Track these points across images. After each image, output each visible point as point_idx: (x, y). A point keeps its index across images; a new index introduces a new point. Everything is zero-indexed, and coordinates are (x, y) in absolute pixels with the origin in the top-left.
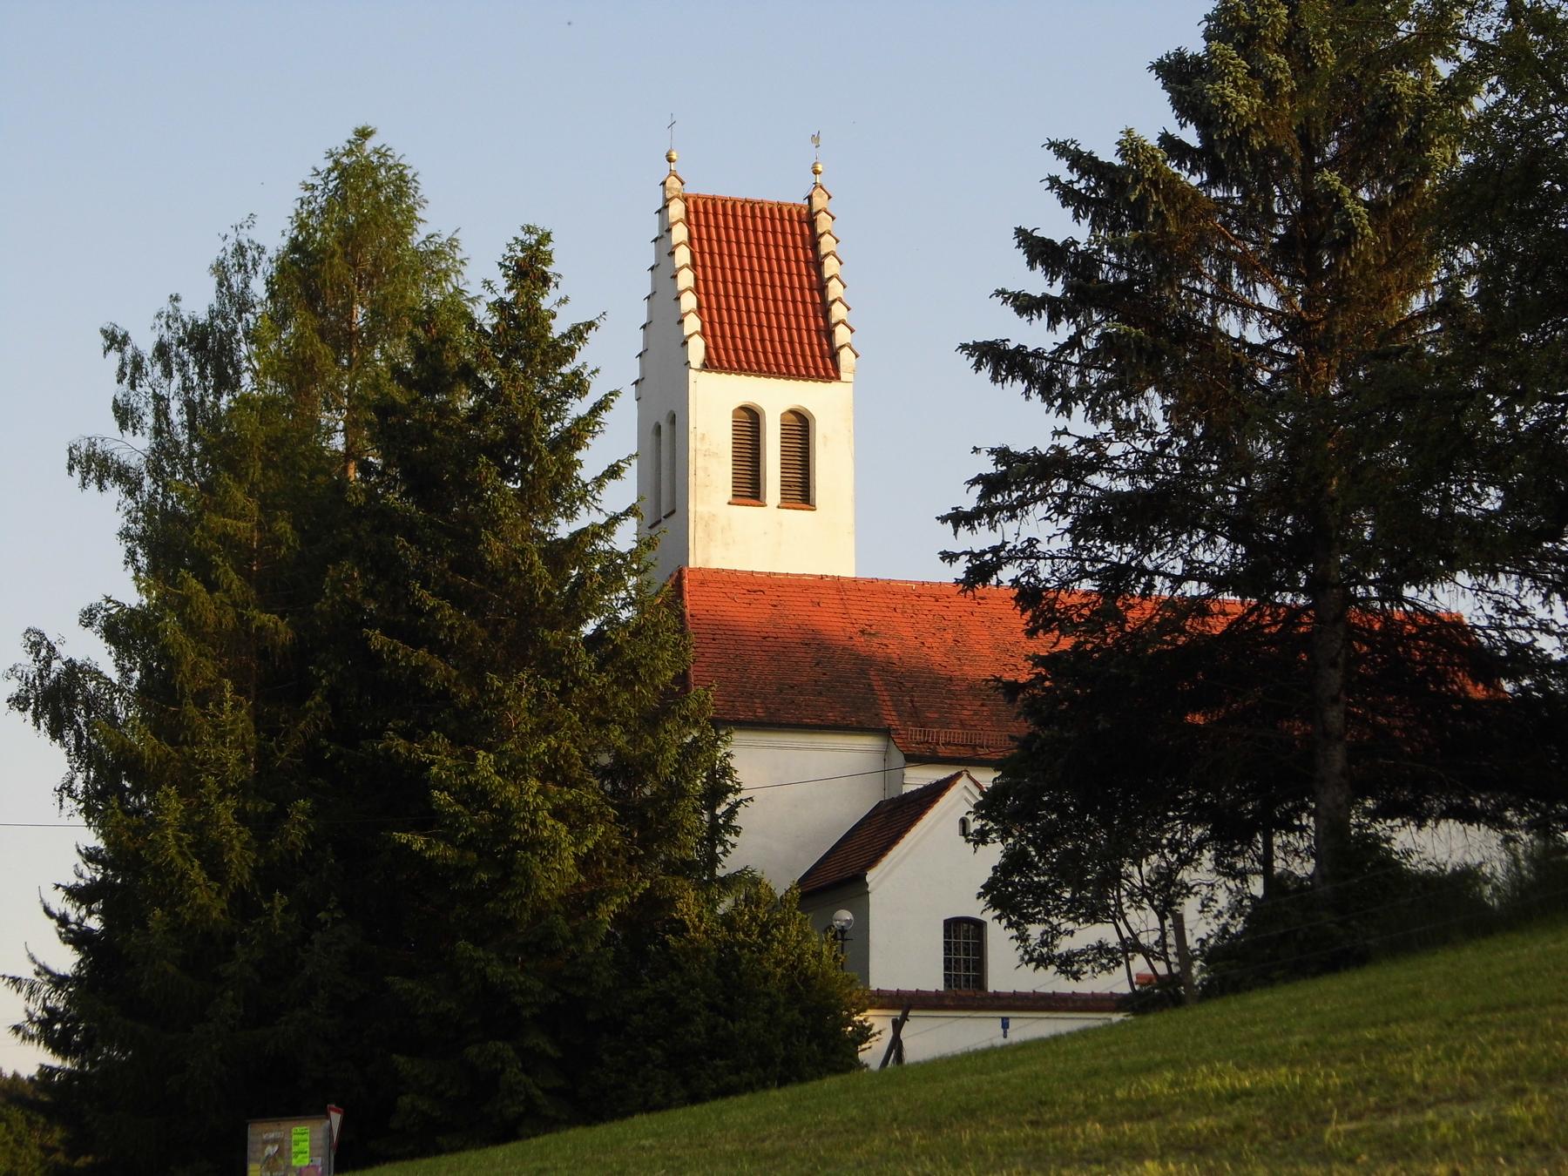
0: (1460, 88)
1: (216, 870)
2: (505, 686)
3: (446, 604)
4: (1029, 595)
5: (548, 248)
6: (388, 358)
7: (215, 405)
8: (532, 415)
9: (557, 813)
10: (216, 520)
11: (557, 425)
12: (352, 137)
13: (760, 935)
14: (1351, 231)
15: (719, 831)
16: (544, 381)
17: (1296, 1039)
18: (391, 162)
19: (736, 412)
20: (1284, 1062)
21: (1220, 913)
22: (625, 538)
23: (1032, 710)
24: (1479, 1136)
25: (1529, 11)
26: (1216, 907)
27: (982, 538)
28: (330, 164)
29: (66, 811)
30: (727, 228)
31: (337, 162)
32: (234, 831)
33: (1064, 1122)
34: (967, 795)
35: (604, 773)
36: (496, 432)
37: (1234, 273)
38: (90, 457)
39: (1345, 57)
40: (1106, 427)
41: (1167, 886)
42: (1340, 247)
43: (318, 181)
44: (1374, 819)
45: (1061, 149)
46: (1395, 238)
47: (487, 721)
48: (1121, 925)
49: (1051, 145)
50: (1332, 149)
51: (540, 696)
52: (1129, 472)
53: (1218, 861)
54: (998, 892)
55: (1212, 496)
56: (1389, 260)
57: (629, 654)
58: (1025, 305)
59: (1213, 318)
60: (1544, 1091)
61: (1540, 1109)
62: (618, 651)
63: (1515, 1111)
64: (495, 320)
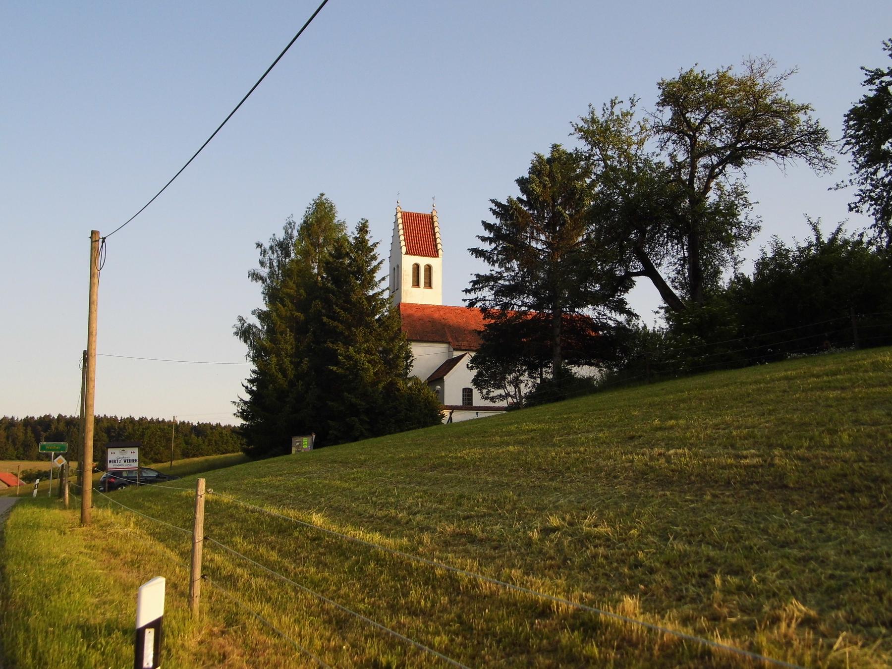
0: (592, 185)
1: (285, 375)
4: (484, 310)
6: (328, 250)
9: (369, 362)
10: (285, 290)
14: (565, 221)
15: (408, 366)
22: (386, 295)
23: (484, 338)
27: (473, 296)
35: (380, 352)
38: (254, 274)
39: (563, 178)
40: (503, 269)
42: (562, 225)
45: (493, 201)
50: (560, 201)
51: (365, 333)
52: (509, 280)
53: (529, 375)
54: (475, 382)
57: (387, 324)
58: (484, 239)
59: (530, 243)
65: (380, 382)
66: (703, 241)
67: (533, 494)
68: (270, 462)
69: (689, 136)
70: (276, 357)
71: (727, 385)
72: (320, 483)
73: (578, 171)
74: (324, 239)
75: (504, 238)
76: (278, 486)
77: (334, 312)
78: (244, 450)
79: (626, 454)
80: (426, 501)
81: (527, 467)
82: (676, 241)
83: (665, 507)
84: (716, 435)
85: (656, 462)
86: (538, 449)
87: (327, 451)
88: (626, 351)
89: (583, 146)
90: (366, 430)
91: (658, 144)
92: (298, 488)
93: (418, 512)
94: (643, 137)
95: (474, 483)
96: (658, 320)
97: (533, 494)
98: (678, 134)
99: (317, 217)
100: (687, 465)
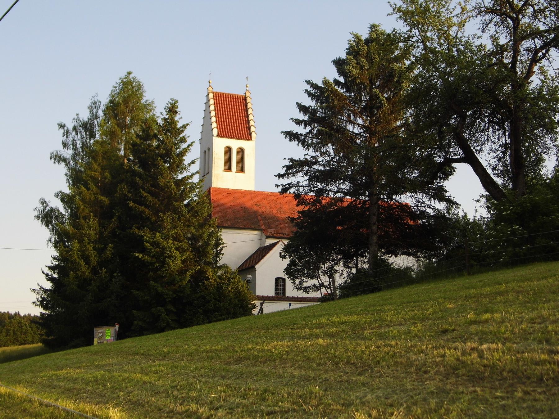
0: (411, 68)
1: (87, 262)
3: (149, 195)
4: (297, 196)
5: (177, 104)
6: (135, 132)
7: (89, 142)
8: (172, 147)
9: (177, 249)
10: (89, 172)
11: (179, 150)
12: (126, 74)
13: (228, 281)
14: (381, 104)
15: (218, 254)
16: (176, 139)
17: (359, 309)
18: (136, 81)
20: (356, 314)
21: (344, 278)
22: (196, 179)
23: (297, 225)
24: (404, 334)
25: (429, 48)
26: (343, 276)
27: (285, 181)
28: (120, 81)
29: (49, 246)
31: (122, 81)
32: (92, 252)
33: (299, 329)
35: (189, 239)
36: (163, 151)
37: (352, 115)
38: (56, 156)
39: (381, 59)
40: (318, 153)
41: (331, 270)
42: (379, 108)
43: (117, 85)
44: (384, 255)
45: (308, 82)
46: (393, 106)
47: (159, 225)
48: (319, 280)
49: (306, 81)
50: (378, 83)
51: (173, 219)
52: (324, 165)
53: (344, 265)
54: (288, 271)
55: (344, 172)
56: (391, 112)
57: (196, 209)
58: (298, 122)
59: (346, 126)
60: (421, 323)
61: (419, 328)
62: (193, 208)
63: (413, 328)
64: (163, 123)
65: (187, 270)
66: (526, 127)
67: (340, 389)
68: (68, 354)
69: (512, 18)
70: (79, 242)
71: (546, 278)
72: (119, 376)
73: (397, 53)
74: (131, 120)
75: (320, 121)
76: (76, 379)
78: (43, 341)
79: (437, 348)
80: (229, 396)
81: (336, 361)
82: (497, 127)
83: (475, 403)
84: (531, 329)
85: (469, 357)
86: (348, 342)
87: (129, 343)
88: (446, 241)
89: (402, 27)
90: (172, 320)
91: (479, 26)
92: (96, 381)
93: (221, 407)
94: (464, 18)
95: (280, 377)
96: (479, 209)
97: (340, 389)
98: (501, 16)
99: (124, 97)
100: (499, 360)
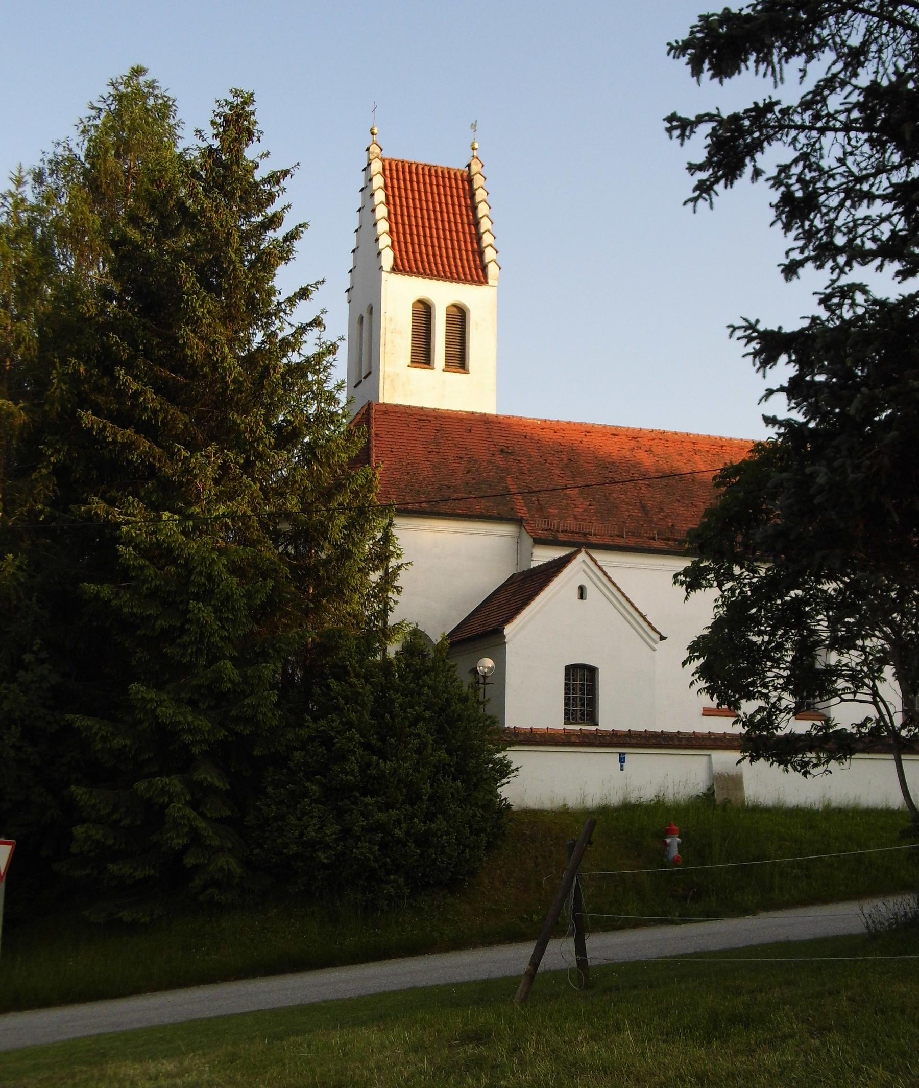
2: (191, 457)
18: (156, 92)
19: (414, 304)
30: (411, 181)
34: (584, 567)
51: (224, 467)
77: (120, 395)
